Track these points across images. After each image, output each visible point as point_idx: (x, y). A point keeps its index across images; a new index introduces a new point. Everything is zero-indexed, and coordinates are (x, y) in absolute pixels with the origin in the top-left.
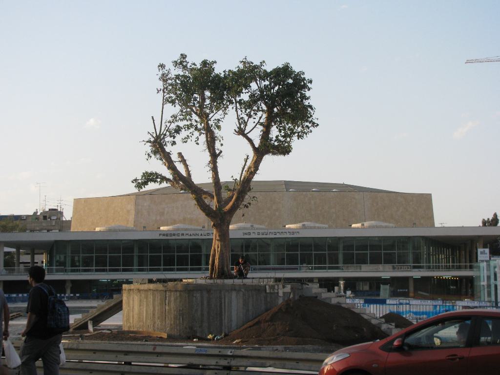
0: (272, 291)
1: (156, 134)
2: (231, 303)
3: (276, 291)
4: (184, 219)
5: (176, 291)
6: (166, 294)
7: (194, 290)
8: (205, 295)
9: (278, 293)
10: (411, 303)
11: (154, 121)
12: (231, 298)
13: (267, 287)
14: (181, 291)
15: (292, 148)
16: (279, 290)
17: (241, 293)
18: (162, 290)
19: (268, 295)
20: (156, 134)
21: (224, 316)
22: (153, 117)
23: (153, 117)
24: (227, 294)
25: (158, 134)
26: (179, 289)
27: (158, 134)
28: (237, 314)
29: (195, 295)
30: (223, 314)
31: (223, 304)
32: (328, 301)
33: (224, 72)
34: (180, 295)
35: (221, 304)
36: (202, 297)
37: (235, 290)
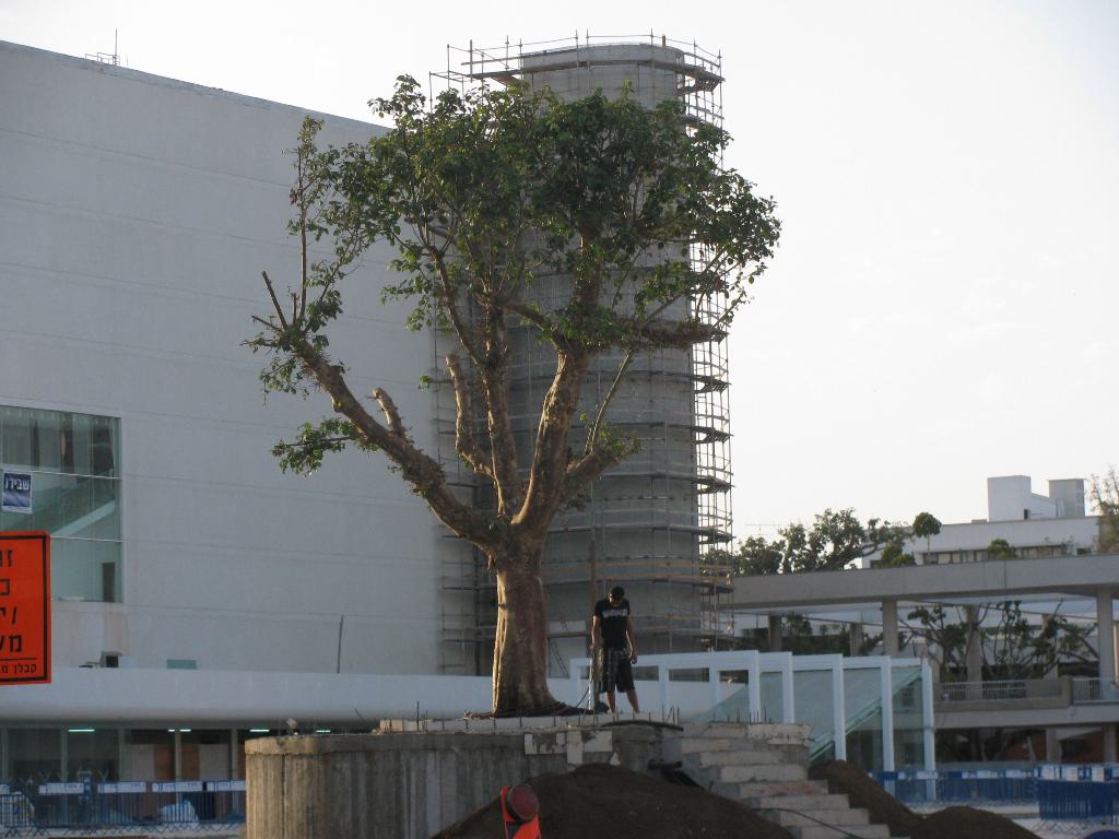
0: (543, 749)
1: (283, 321)
2: (425, 786)
3: (558, 750)
4: (1107, 491)
5: (301, 756)
6: (283, 765)
7: (335, 752)
8: (363, 765)
9: (565, 755)
10: (710, 420)
11: (268, 283)
12: (425, 772)
13: (528, 739)
14: (310, 756)
15: (733, 170)
16: (570, 746)
17: (452, 758)
18: (276, 755)
19: (533, 761)
20: (283, 321)
21: (406, 824)
22: (264, 274)
23: (264, 274)
24: (413, 761)
25: (289, 321)
26: (307, 752)
27: (289, 321)
28: (441, 817)
29: (338, 766)
30: (406, 817)
31: (405, 791)
32: (770, 817)
33: (886, 523)
34: (310, 766)
35: (399, 789)
36: (354, 772)
37: (434, 750)
